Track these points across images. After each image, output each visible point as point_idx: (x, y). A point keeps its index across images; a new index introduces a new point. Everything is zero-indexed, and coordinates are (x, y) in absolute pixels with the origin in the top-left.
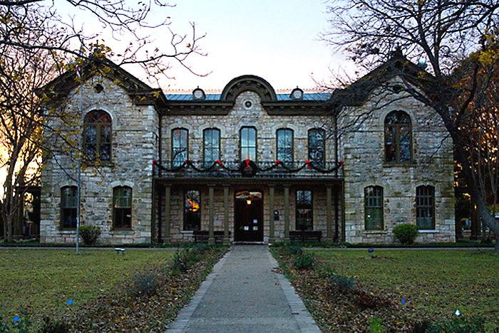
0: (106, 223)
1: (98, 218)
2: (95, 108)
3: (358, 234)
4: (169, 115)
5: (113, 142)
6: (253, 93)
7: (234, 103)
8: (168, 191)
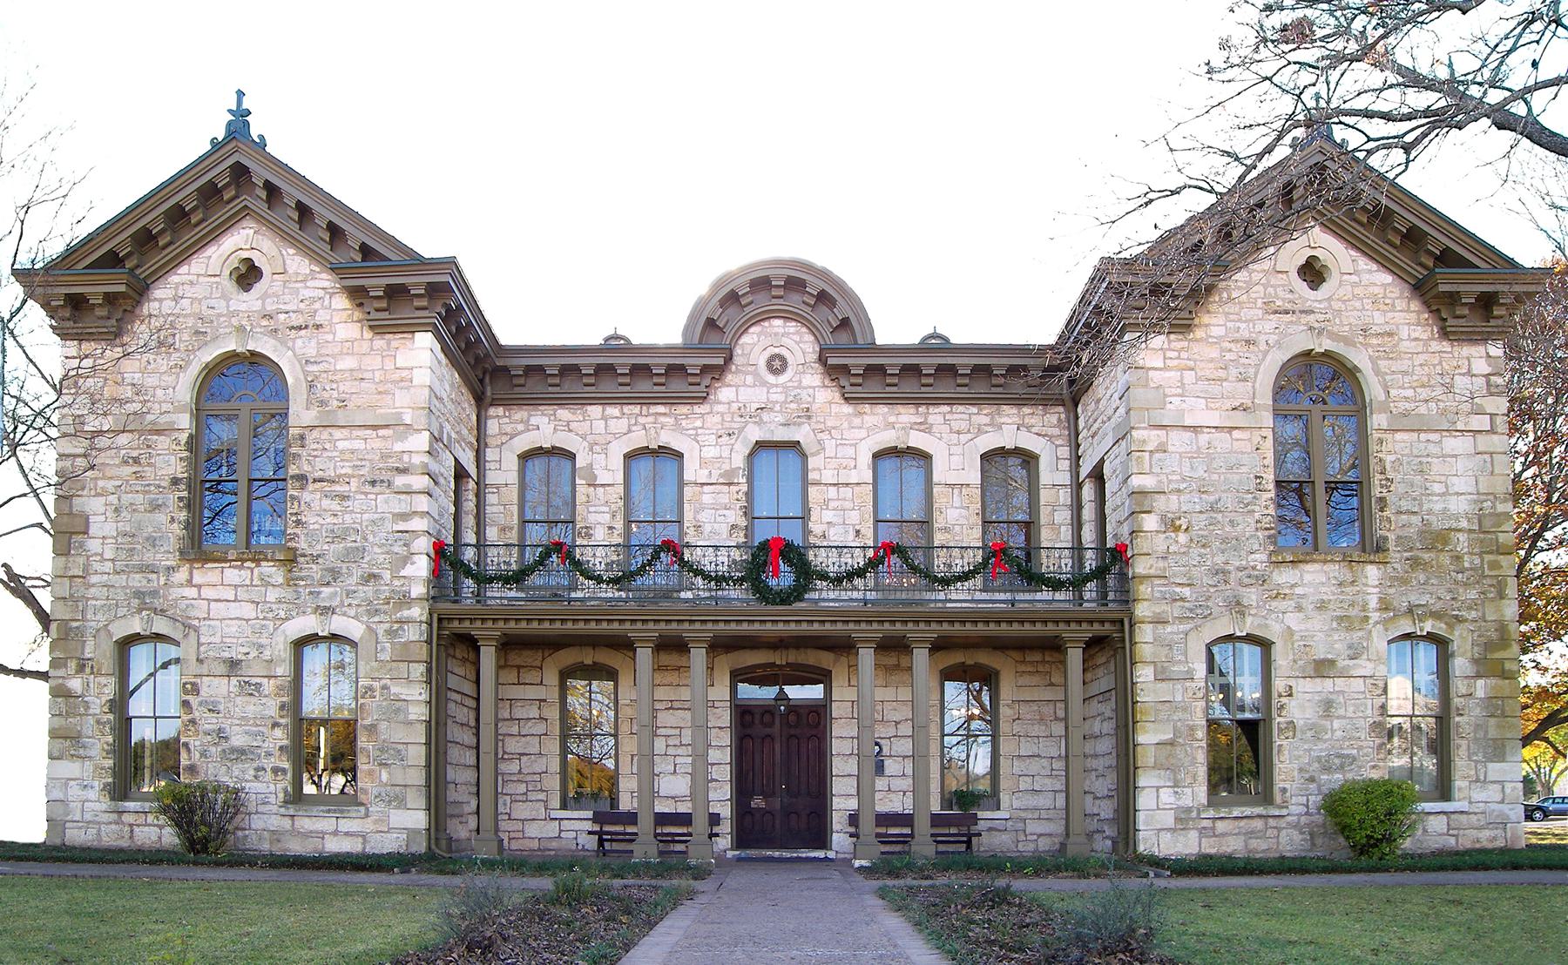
0: (269, 775)
1: (241, 753)
2: (232, 347)
3: (1183, 819)
4: (507, 403)
5: (293, 470)
6: (792, 327)
7: (729, 359)
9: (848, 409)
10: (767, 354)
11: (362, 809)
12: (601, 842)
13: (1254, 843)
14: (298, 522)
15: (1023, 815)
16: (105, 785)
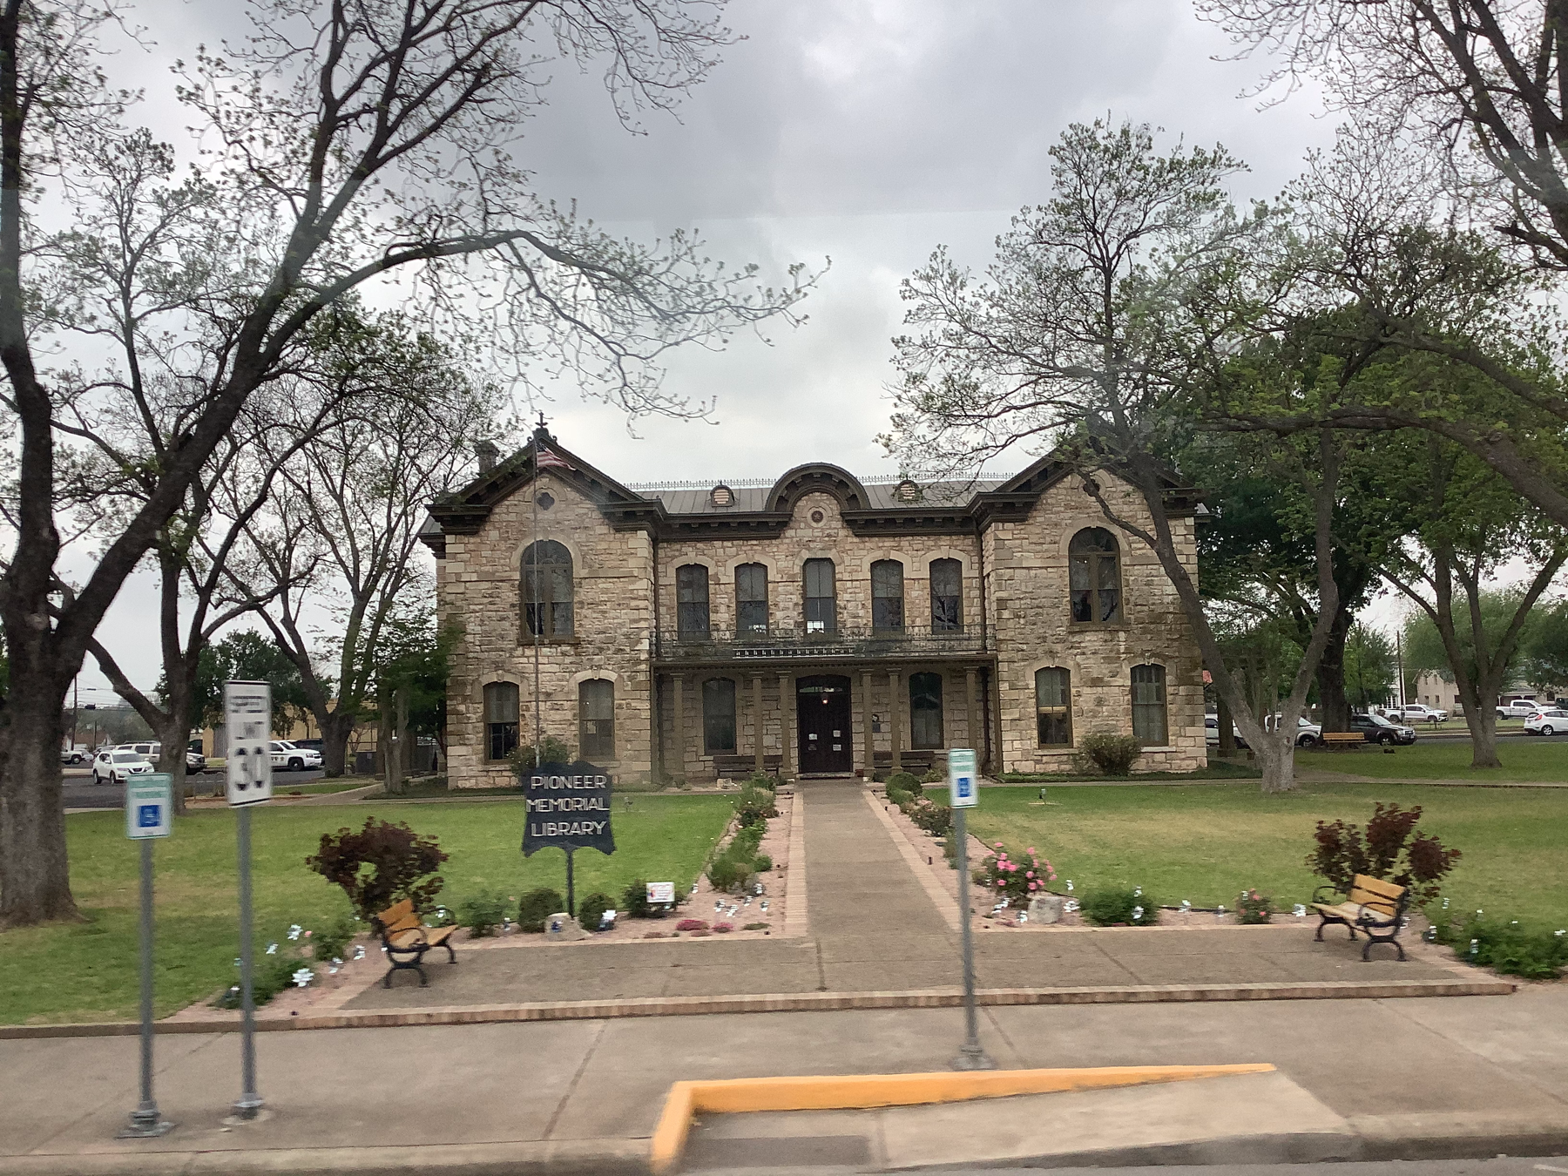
5: (576, 599)
9: (856, 540)
10: (812, 511)
13: (1063, 767)
14: (581, 625)
16: (480, 759)
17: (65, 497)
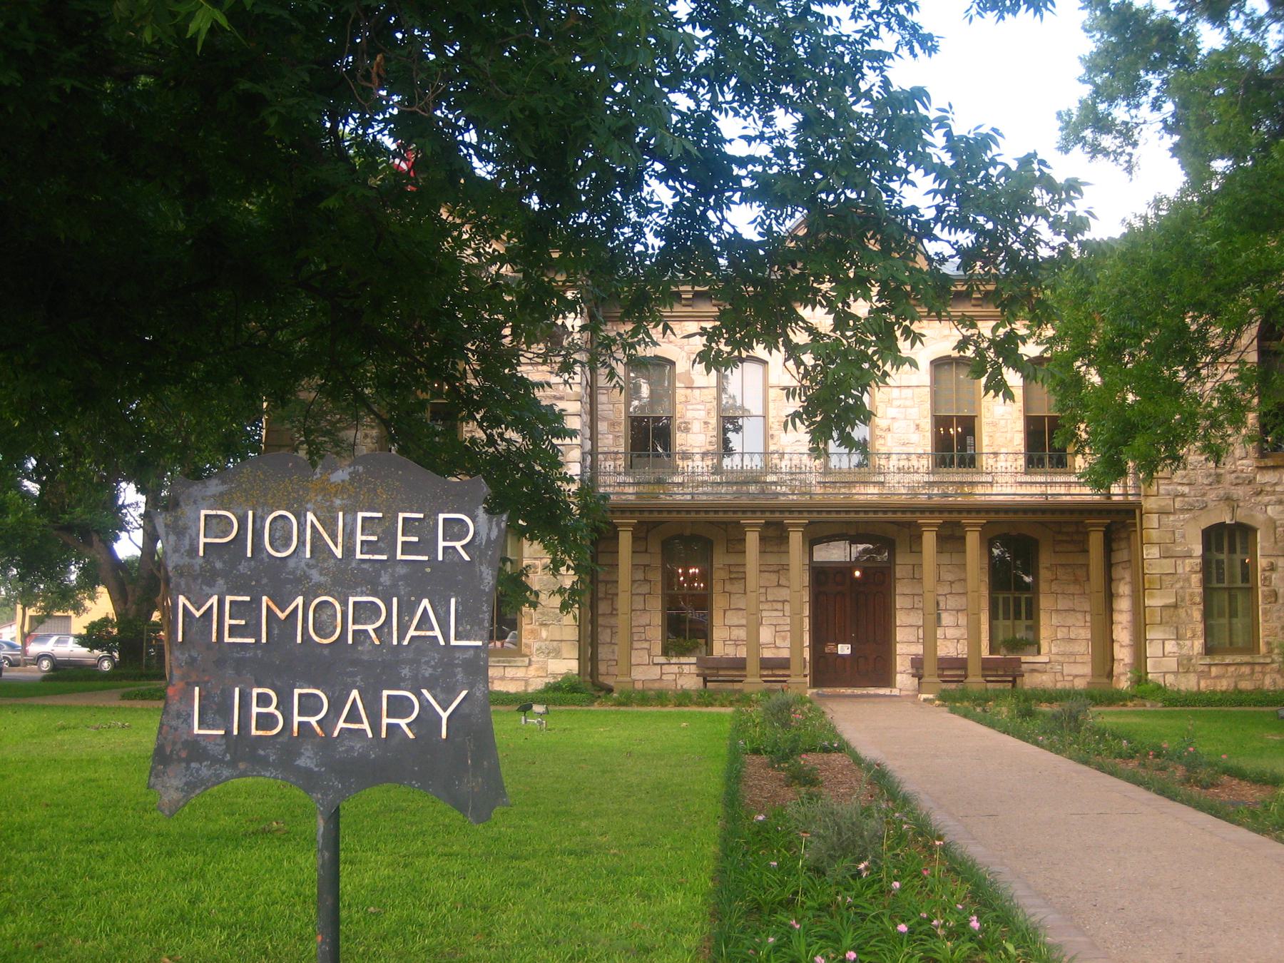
3: (1185, 665)
8: (625, 539)
11: (527, 660)
12: (705, 681)
15: (1060, 659)
17: (1101, 733)
